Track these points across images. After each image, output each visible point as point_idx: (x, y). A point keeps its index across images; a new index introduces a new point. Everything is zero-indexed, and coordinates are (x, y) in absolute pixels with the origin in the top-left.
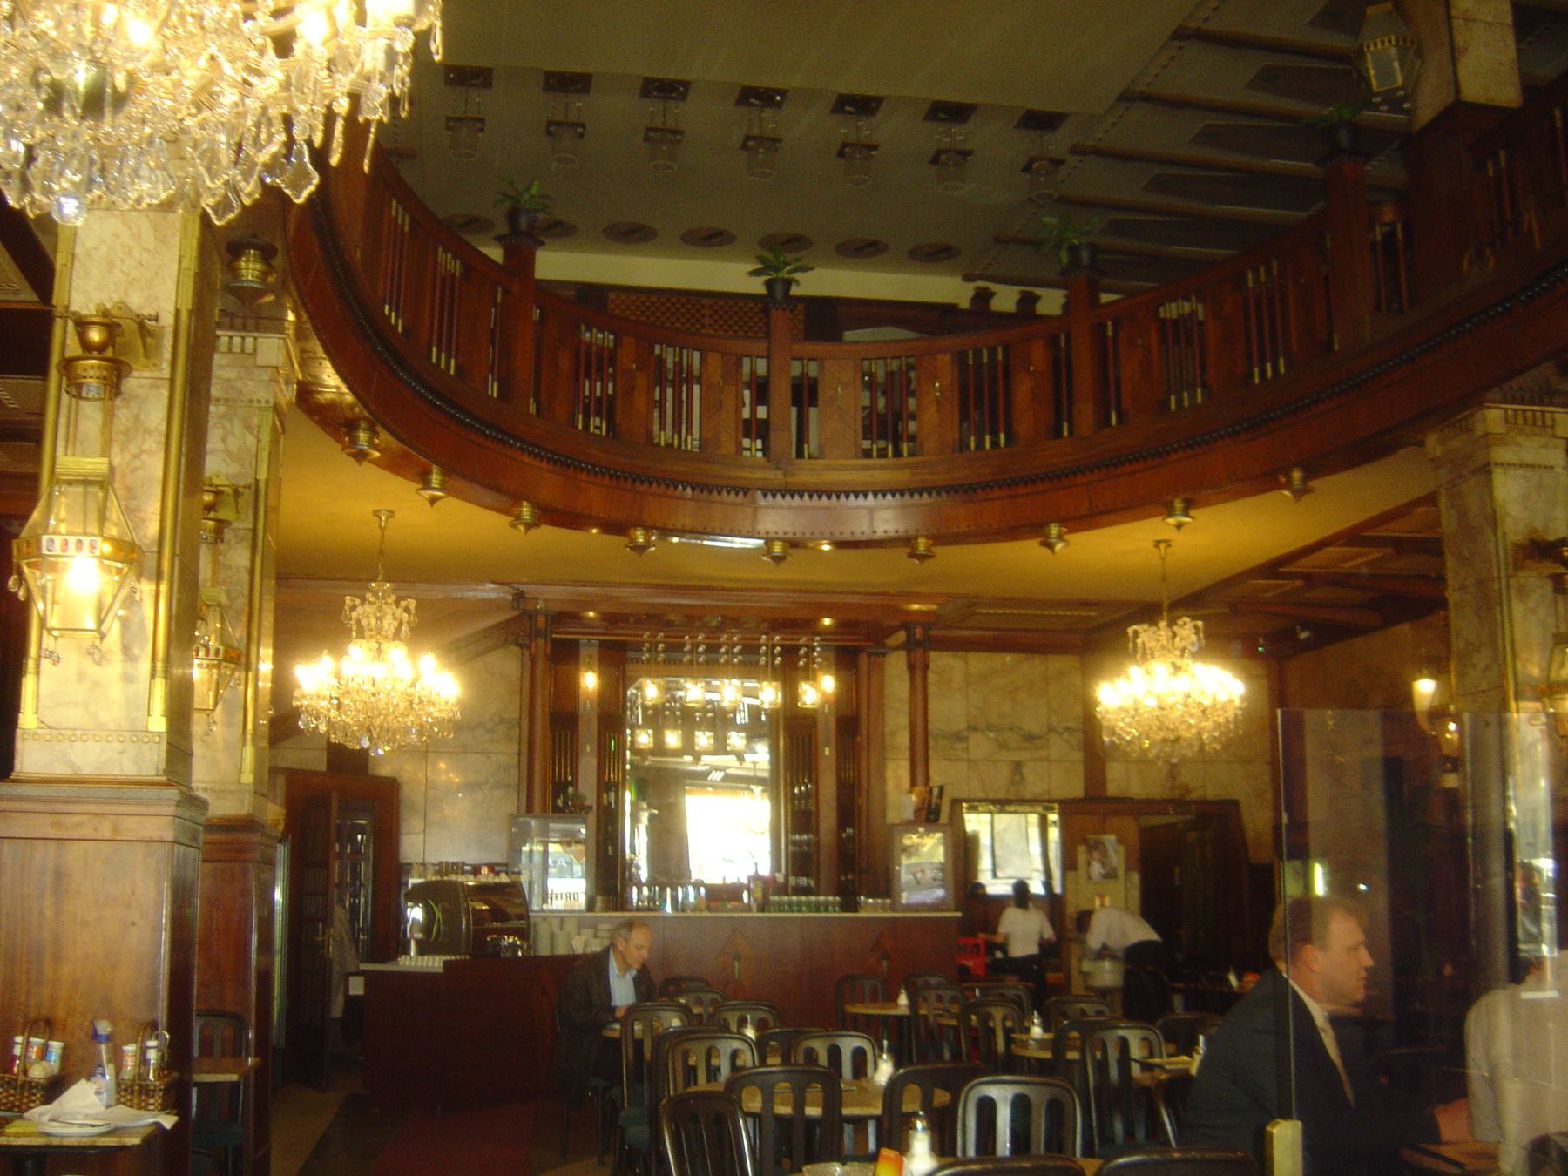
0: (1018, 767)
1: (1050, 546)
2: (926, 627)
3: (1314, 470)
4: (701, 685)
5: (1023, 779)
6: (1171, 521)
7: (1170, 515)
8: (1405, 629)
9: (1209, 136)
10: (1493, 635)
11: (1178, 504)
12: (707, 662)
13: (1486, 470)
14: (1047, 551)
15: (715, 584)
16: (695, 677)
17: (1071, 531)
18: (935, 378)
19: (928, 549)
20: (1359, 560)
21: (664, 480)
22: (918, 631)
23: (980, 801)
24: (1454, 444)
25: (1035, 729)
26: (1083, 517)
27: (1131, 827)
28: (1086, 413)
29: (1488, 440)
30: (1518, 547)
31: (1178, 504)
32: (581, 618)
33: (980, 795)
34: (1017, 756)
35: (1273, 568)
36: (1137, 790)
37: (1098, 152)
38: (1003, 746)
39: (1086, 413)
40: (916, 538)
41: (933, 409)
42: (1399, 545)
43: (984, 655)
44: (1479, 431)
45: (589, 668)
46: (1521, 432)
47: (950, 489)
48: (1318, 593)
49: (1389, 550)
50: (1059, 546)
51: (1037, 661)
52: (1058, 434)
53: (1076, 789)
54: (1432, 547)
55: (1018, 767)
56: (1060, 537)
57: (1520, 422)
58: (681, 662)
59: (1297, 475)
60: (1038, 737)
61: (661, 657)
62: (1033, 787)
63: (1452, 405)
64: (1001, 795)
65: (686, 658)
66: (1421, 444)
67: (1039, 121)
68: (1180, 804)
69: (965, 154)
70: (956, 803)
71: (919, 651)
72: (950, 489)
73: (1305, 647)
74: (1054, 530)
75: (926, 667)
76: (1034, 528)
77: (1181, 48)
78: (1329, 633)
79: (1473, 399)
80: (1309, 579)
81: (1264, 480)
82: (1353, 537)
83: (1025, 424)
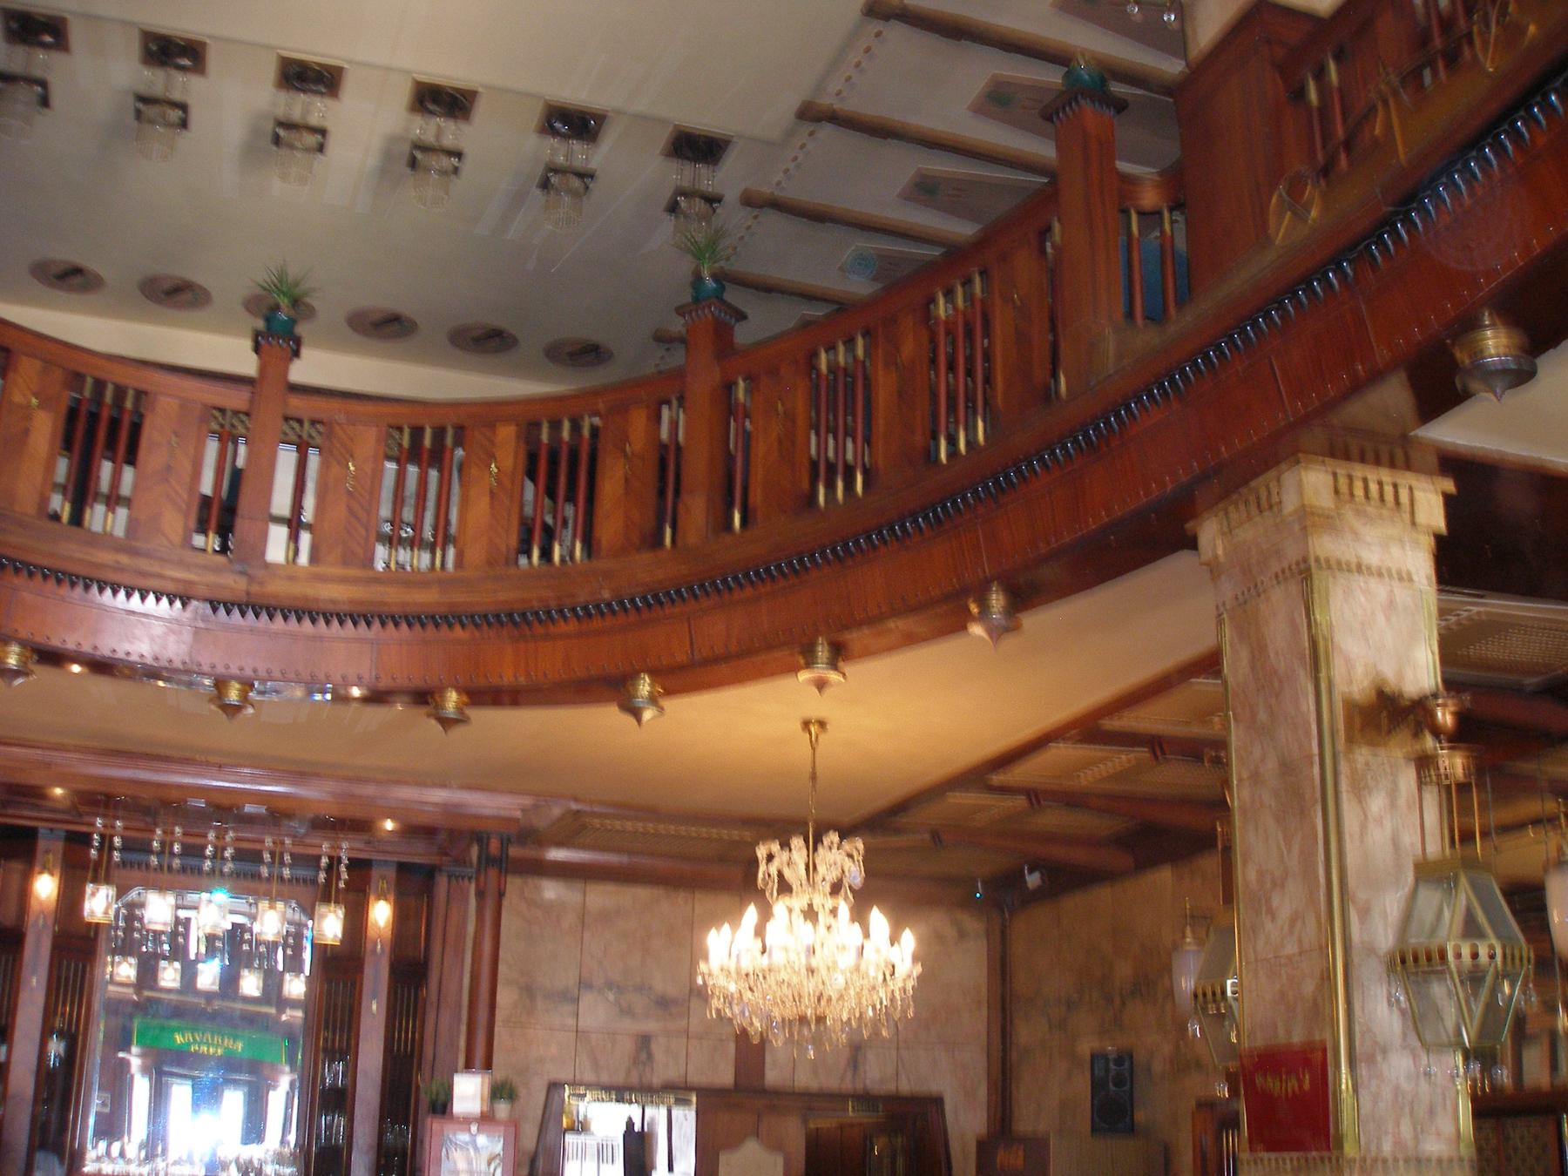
0: (644, 1041)
1: (636, 713)
2: (506, 842)
3: (1023, 598)
4: (171, 899)
5: (650, 1056)
6: (804, 676)
7: (810, 664)
8: (1164, 876)
9: (925, 190)
10: (1307, 857)
11: (822, 652)
12: (183, 870)
13: (1304, 574)
14: (631, 720)
15: (168, 752)
16: (162, 888)
17: (669, 692)
18: (492, 456)
19: (459, 709)
20: (1098, 767)
21: (27, 564)
22: (494, 846)
23: (589, 1086)
24: (1246, 534)
25: (672, 991)
26: (682, 668)
27: (794, 1132)
28: (696, 509)
29: (1309, 520)
30: (1351, 707)
31: (822, 652)
32: (44, 797)
33: (589, 1076)
34: (651, 1026)
35: (981, 775)
36: (804, 1080)
37: (777, 205)
38: (626, 1011)
39: (696, 509)
40: (441, 690)
41: (484, 501)
42: (1157, 745)
43: (610, 888)
44: (1290, 503)
45: (382, 896)
46: (1360, 513)
47: (814, 768)
48: (1051, 819)
49: (1143, 753)
50: (648, 715)
51: (681, 897)
52: (656, 541)
53: (725, 1076)
54: (1207, 752)
55: (644, 1041)
56: (653, 700)
57: (1359, 491)
58: (200, 871)
59: (997, 600)
60: (675, 1002)
61: (177, 862)
62: (665, 1069)
63: (1239, 471)
64: (620, 1079)
65: (208, 864)
66: (1192, 544)
67: (696, 147)
68: (866, 1099)
69: (586, 176)
70: (554, 1087)
71: (493, 873)
72: (814, 768)
73: (1031, 899)
74: (645, 687)
75: (501, 895)
76: (612, 687)
77: (878, 35)
78: (1066, 879)
79: (1275, 453)
80: (1035, 796)
81: (946, 612)
82: (1089, 729)
83: (609, 529)
